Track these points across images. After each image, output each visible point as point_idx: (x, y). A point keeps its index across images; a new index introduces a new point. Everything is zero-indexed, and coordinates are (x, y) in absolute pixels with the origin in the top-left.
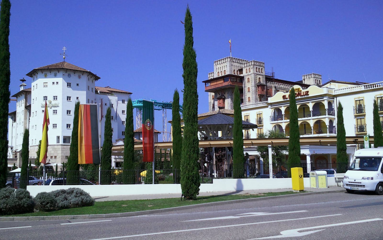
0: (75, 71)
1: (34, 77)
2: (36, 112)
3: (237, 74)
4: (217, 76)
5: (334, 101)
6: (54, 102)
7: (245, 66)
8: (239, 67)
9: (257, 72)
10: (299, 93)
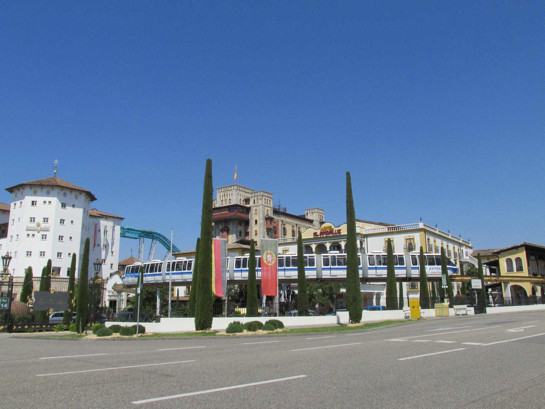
0: (72, 190)
1: (16, 193)
2: (18, 235)
3: (243, 204)
4: (220, 204)
5: (364, 240)
6: (43, 225)
7: (253, 196)
8: (245, 196)
9: (265, 203)
10: (330, 231)
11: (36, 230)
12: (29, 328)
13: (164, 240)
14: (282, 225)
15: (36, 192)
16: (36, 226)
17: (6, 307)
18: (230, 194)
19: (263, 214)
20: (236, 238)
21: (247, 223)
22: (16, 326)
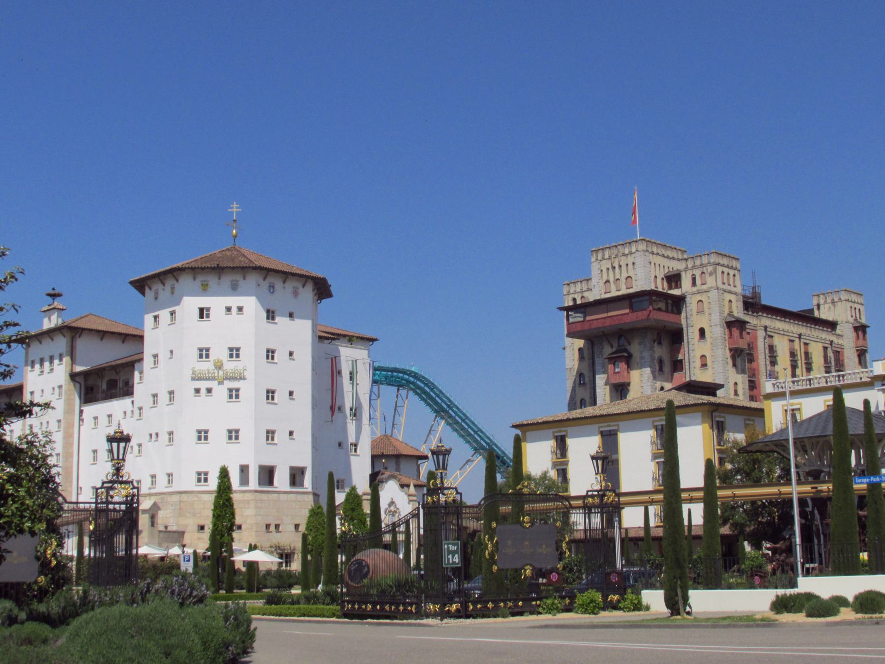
0: (286, 275)
3: (663, 289)
4: (603, 291)
6: (230, 366)
7: (690, 266)
9: (724, 283)
11: (214, 379)
12: (495, 606)
13: (426, 388)
14: (765, 339)
15: (207, 285)
16: (214, 368)
17: (457, 562)
18: (627, 265)
19: (721, 312)
20: (652, 378)
21: (676, 337)
22: (473, 605)
